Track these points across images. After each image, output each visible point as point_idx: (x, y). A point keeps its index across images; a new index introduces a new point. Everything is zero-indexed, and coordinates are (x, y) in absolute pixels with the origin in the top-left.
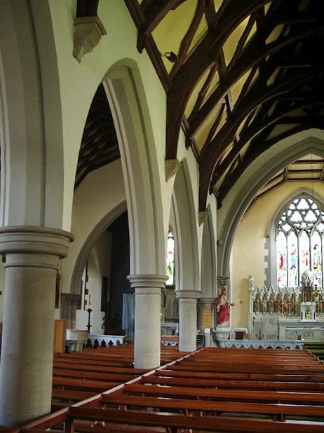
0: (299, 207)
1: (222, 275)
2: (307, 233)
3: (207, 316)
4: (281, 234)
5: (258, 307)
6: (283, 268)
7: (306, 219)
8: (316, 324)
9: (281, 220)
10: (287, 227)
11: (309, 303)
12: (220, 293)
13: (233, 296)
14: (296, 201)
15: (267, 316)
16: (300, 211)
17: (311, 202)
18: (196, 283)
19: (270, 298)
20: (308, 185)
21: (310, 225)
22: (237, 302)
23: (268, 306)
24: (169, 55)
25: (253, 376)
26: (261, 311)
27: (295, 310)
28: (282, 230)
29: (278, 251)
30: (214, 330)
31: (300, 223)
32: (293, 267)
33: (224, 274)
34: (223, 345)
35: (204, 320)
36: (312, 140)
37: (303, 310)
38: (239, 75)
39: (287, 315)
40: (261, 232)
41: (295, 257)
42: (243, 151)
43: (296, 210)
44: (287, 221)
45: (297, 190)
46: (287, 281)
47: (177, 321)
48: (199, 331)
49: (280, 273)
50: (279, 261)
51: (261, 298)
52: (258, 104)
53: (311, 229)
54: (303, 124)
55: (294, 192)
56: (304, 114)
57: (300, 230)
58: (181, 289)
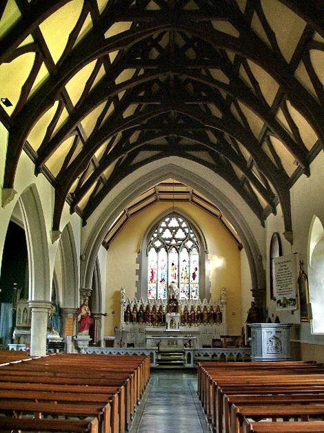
0: (170, 225)
1: (84, 287)
2: (176, 250)
3: (69, 325)
4: (153, 250)
5: (129, 317)
6: (153, 281)
7: (176, 236)
8: (180, 333)
9: (153, 236)
10: (158, 244)
11: (174, 314)
12: (82, 303)
13: (105, 306)
14: (167, 220)
15: (137, 325)
16: (171, 229)
17: (181, 220)
18: (47, 294)
19: (140, 308)
20: (177, 204)
21: (179, 242)
22: (109, 312)
23: (137, 316)
24: (4, 100)
25: (58, 375)
26: (131, 321)
27: (161, 320)
28: (154, 246)
29: (149, 265)
30: (75, 337)
31: (170, 240)
32: (163, 280)
33: (86, 287)
34: (83, 352)
35: (67, 329)
36: (171, 166)
37: (168, 321)
38: (32, 124)
39: (153, 325)
40: (133, 247)
41: (164, 271)
42: (106, 173)
43: (167, 227)
44: (158, 238)
45: (170, 209)
46: (157, 293)
47: (29, 328)
48: (62, 339)
49: (151, 285)
50: (150, 275)
51: (132, 309)
52: (118, 131)
53: (180, 246)
54: (165, 151)
55: (166, 211)
56: (165, 142)
57: (170, 246)
58: (33, 299)
